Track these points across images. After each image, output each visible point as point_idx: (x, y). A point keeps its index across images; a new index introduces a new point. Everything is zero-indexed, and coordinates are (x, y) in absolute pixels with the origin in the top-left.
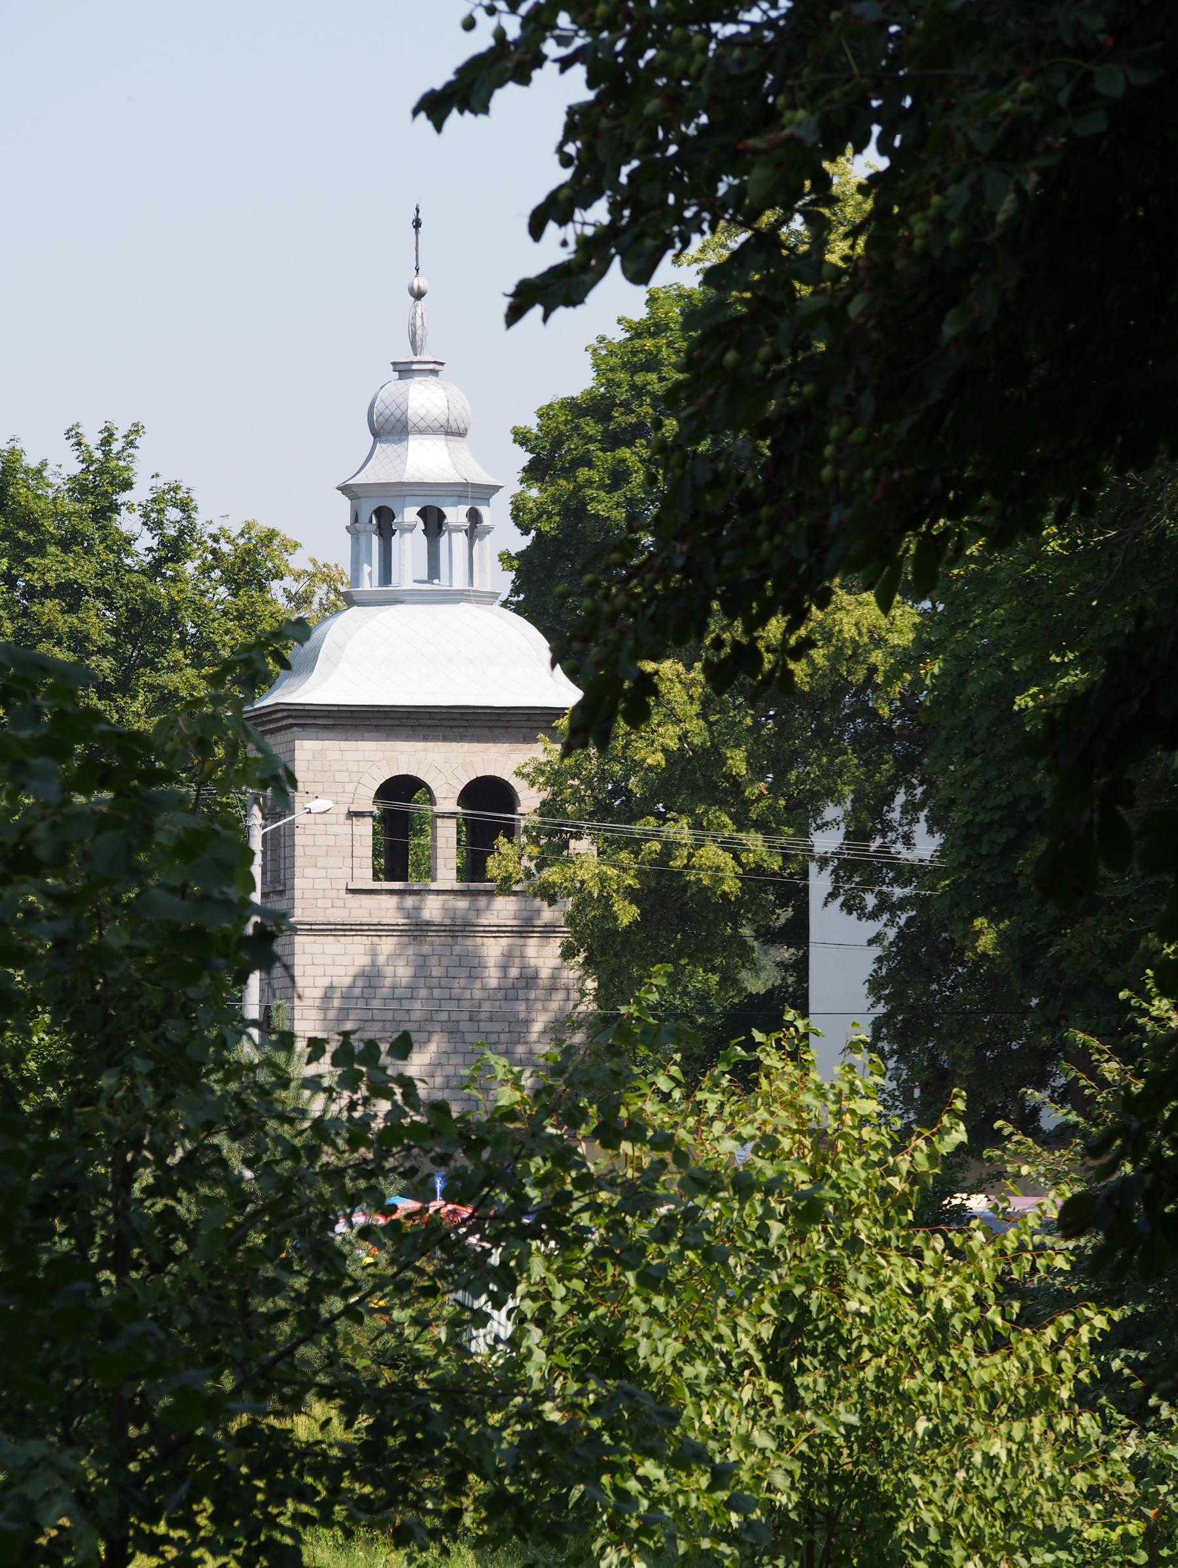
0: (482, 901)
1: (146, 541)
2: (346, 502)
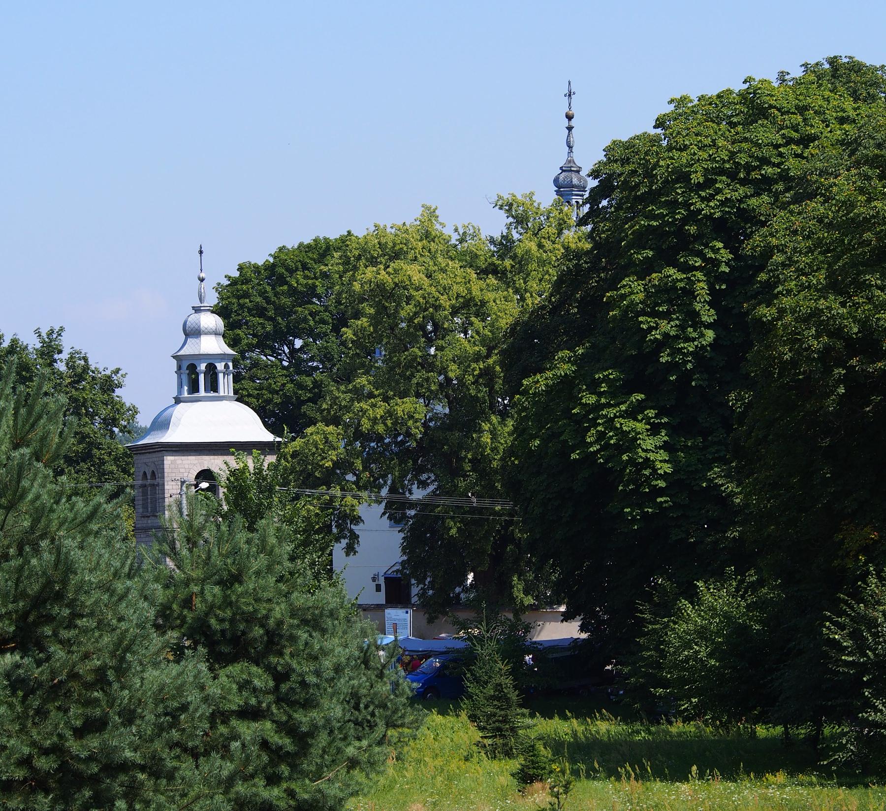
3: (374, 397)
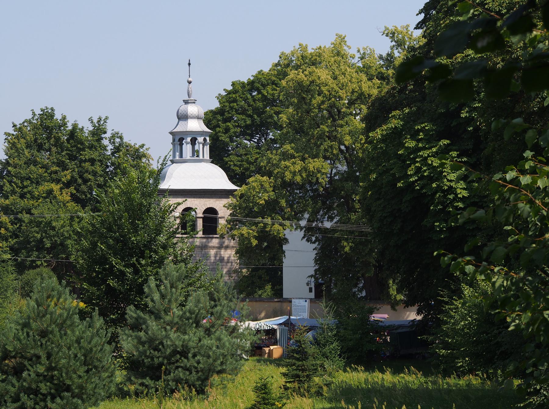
0: (210, 240)
1: (110, 147)
2: (171, 137)
3: (295, 158)
